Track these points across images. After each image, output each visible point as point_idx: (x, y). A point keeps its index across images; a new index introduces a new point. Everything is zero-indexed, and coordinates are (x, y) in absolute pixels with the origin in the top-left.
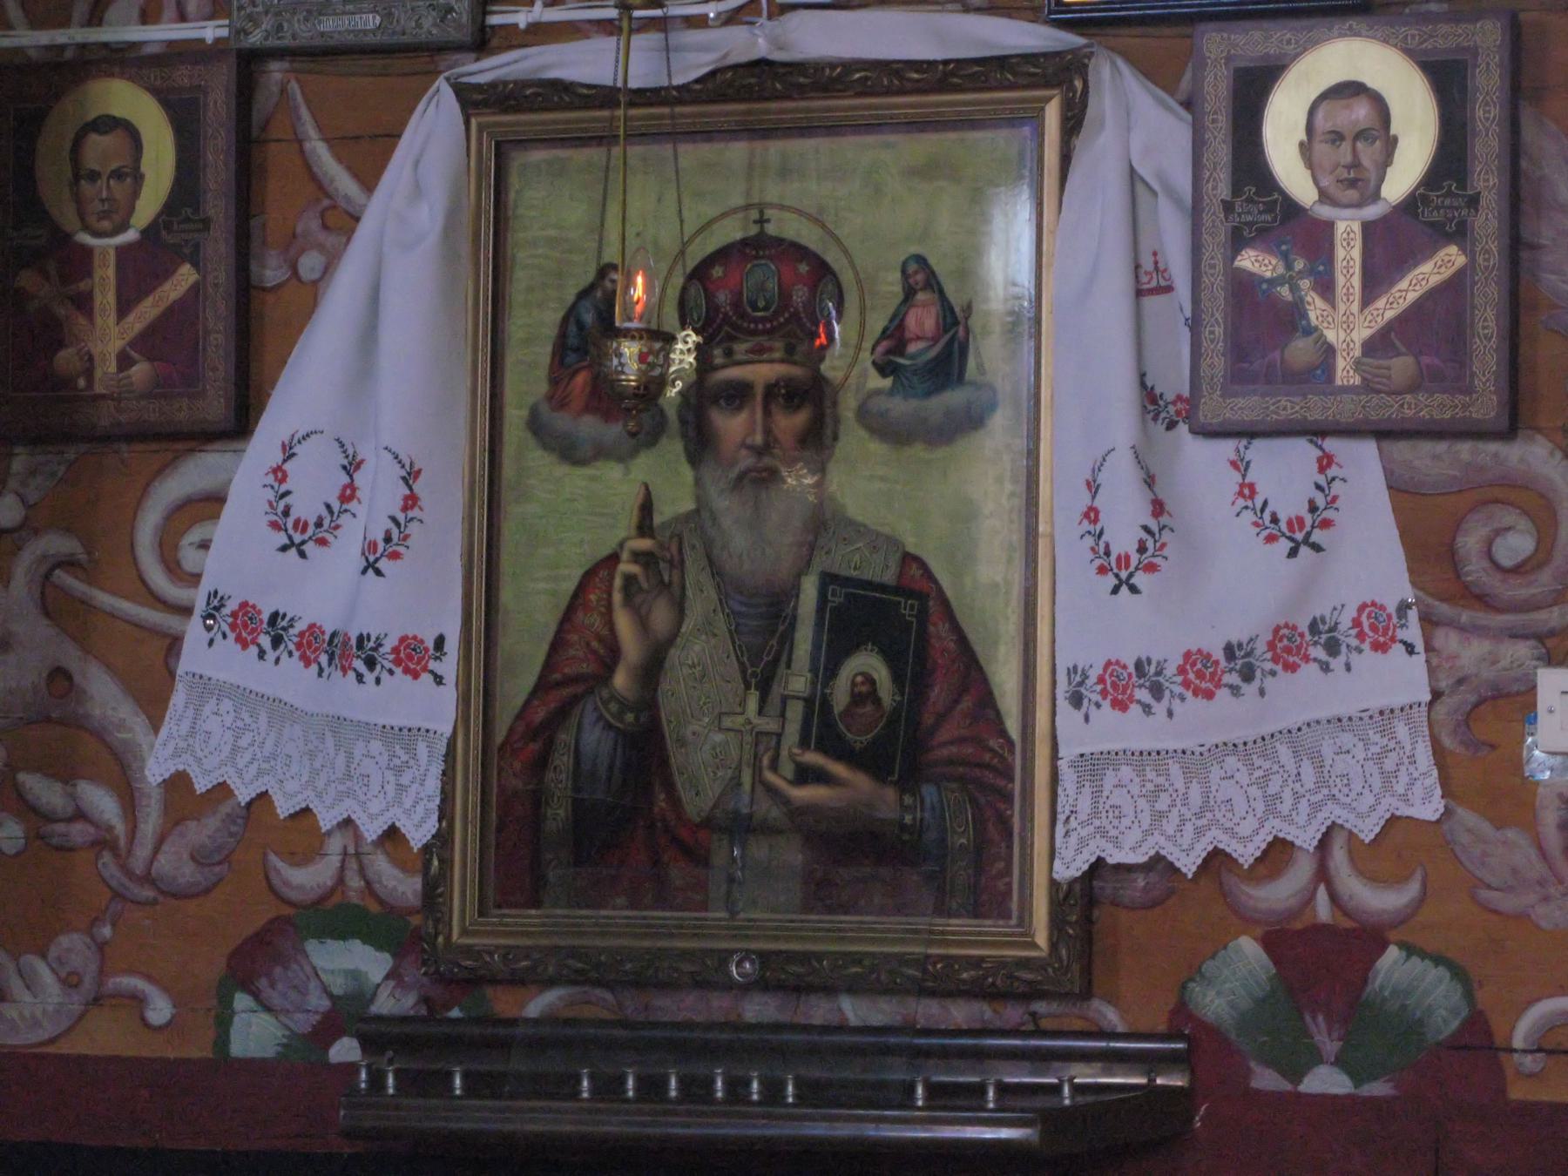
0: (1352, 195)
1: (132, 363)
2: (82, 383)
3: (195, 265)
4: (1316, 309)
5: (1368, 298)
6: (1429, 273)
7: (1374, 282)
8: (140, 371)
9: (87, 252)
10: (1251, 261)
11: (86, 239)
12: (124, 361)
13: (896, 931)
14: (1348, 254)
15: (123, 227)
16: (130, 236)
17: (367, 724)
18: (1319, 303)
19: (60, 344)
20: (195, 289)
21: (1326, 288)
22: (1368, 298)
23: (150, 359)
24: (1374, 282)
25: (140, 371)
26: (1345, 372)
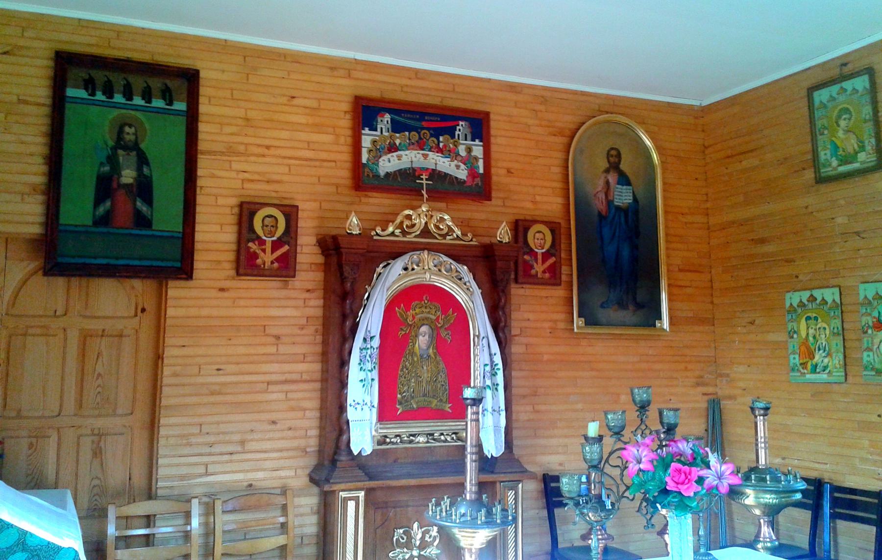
0: (540, 248)
1: (274, 263)
2: (262, 266)
3: (289, 245)
4: (535, 265)
5: (272, 252)
6: (552, 260)
7: (544, 262)
8: (276, 265)
9: (537, 253)
10: (526, 257)
11: (536, 250)
12: (272, 263)
13: (267, 529)
14: (540, 257)
15: (273, 236)
16: (274, 238)
17: (868, 403)
18: (263, 254)
19: (257, 258)
20: (288, 251)
21: (537, 263)
22: (272, 252)
23: (549, 273)
24: (544, 262)
25: (276, 265)
26: (539, 275)
